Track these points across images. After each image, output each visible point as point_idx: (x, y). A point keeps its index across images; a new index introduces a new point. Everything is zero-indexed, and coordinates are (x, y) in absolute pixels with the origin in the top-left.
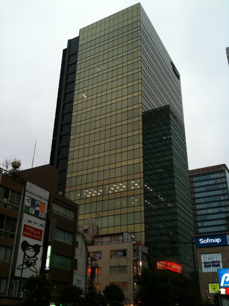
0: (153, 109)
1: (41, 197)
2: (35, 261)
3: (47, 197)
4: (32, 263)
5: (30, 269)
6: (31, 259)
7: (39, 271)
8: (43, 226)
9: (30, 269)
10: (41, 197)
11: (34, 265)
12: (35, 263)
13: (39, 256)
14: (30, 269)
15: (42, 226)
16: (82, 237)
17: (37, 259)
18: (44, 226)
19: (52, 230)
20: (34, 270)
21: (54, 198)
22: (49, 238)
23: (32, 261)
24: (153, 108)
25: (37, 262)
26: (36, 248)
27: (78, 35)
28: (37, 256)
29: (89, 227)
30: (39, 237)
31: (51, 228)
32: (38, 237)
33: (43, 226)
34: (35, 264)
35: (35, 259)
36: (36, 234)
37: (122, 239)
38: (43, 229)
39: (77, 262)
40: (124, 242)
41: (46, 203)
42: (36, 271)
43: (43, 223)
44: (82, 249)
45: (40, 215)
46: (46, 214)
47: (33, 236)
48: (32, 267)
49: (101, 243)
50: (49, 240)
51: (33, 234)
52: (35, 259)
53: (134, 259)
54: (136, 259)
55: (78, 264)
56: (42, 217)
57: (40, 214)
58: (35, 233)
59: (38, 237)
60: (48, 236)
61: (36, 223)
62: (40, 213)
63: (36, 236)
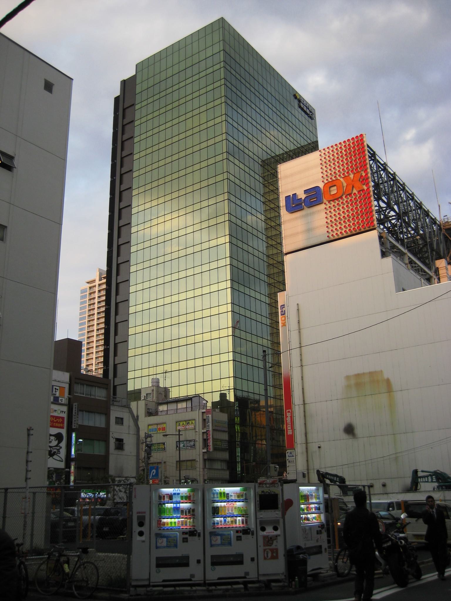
0: (298, 148)
1: (59, 381)
2: (58, 450)
3: (68, 380)
4: (55, 452)
5: (54, 459)
6: (53, 448)
7: (65, 459)
8: (65, 412)
9: (53, 458)
10: (59, 381)
11: (58, 454)
12: (59, 452)
13: (63, 444)
14: (54, 459)
15: (63, 412)
16: (128, 411)
17: (61, 448)
18: (66, 413)
19: (75, 415)
20: (59, 459)
21: (76, 378)
22: (73, 425)
23: (55, 450)
24: (299, 146)
25: (61, 450)
26: (59, 437)
27: (134, 73)
28: (61, 445)
29: (153, 391)
30: (61, 425)
31: (74, 414)
32: (59, 425)
33: (65, 412)
34: (59, 453)
35: (58, 448)
36: (57, 422)
37: (190, 406)
38: (65, 415)
39: (123, 442)
40: (193, 410)
41: (67, 386)
42: (61, 459)
43: (65, 409)
44: (129, 426)
45: (60, 401)
46: (67, 398)
47: (53, 424)
48: (55, 457)
49: (166, 412)
50: (73, 427)
51: (53, 423)
52: (58, 448)
53: (203, 431)
54: (205, 431)
55: (125, 443)
56: (63, 402)
57: (60, 400)
58: (55, 421)
59: (59, 425)
60: (72, 422)
61: (56, 410)
62: (60, 399)
63: (57, 424)
